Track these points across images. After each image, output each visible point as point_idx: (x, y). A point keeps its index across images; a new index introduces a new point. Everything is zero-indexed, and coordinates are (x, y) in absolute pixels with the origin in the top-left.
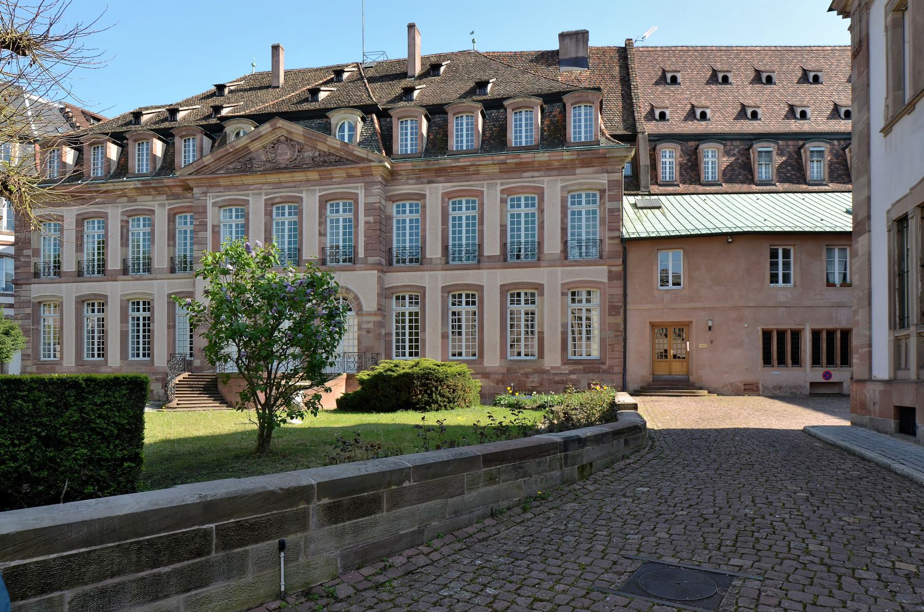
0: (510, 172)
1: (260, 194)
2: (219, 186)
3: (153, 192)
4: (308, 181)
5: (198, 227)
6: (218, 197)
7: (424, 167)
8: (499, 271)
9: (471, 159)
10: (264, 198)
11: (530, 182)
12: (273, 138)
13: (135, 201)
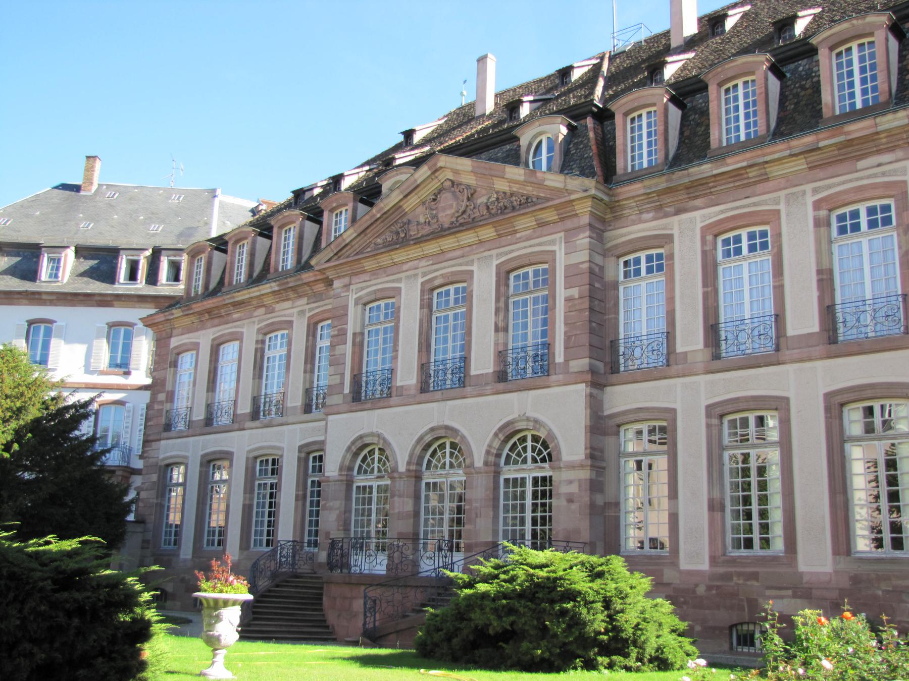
0: (829, 164)
1: (416, 275)
2: (364, 272)
3: (292, 295)
4: (481, 242)
5: (335, 340)
6: (362, 289)
7: (664, 185)
8: (820, 365)
9: (748, 155)
10: (421, 280)
11: (875, 176)
12: (434, 185)
13: (273, 311)
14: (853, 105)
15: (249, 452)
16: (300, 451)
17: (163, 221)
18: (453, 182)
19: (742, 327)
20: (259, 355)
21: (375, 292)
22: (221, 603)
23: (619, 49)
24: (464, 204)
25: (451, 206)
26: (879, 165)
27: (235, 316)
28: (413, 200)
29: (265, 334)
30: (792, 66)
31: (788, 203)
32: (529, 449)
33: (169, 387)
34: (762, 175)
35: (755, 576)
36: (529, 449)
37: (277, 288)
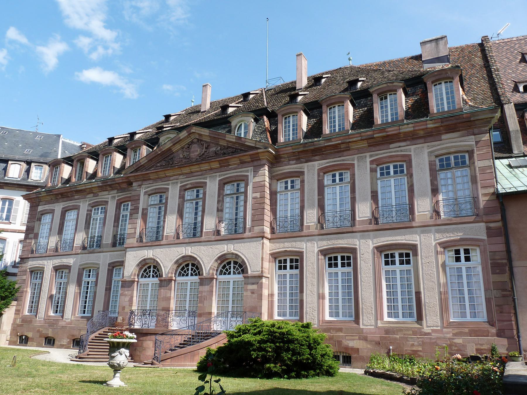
0: (378, 145)
1: (177, 182)
2: (150, 179)
6: (148, 187)
10: (179, 185)
11: (398, 151)
12: (189, 140)
14: (387, 120)
15: (80, 265)
16: (109, 266)
17: (32, 148)
18: (198, 139)
19: (286, 220)
20: (88, 217)
21: (155, 189)
22: (121, 345)
23: (269, 88)
24: (204, 150)
25: (197, 151)
26: (400, 147)
27: (76, 197)
28: (178, 147)
29: (92, 207)
30: (358, 101)
31: (358, 161)
32: (190, 269)
33: (35, 231)
34: (347, 147)
35: (340, 330)
36: (190, 269)
37: (101, 185)
